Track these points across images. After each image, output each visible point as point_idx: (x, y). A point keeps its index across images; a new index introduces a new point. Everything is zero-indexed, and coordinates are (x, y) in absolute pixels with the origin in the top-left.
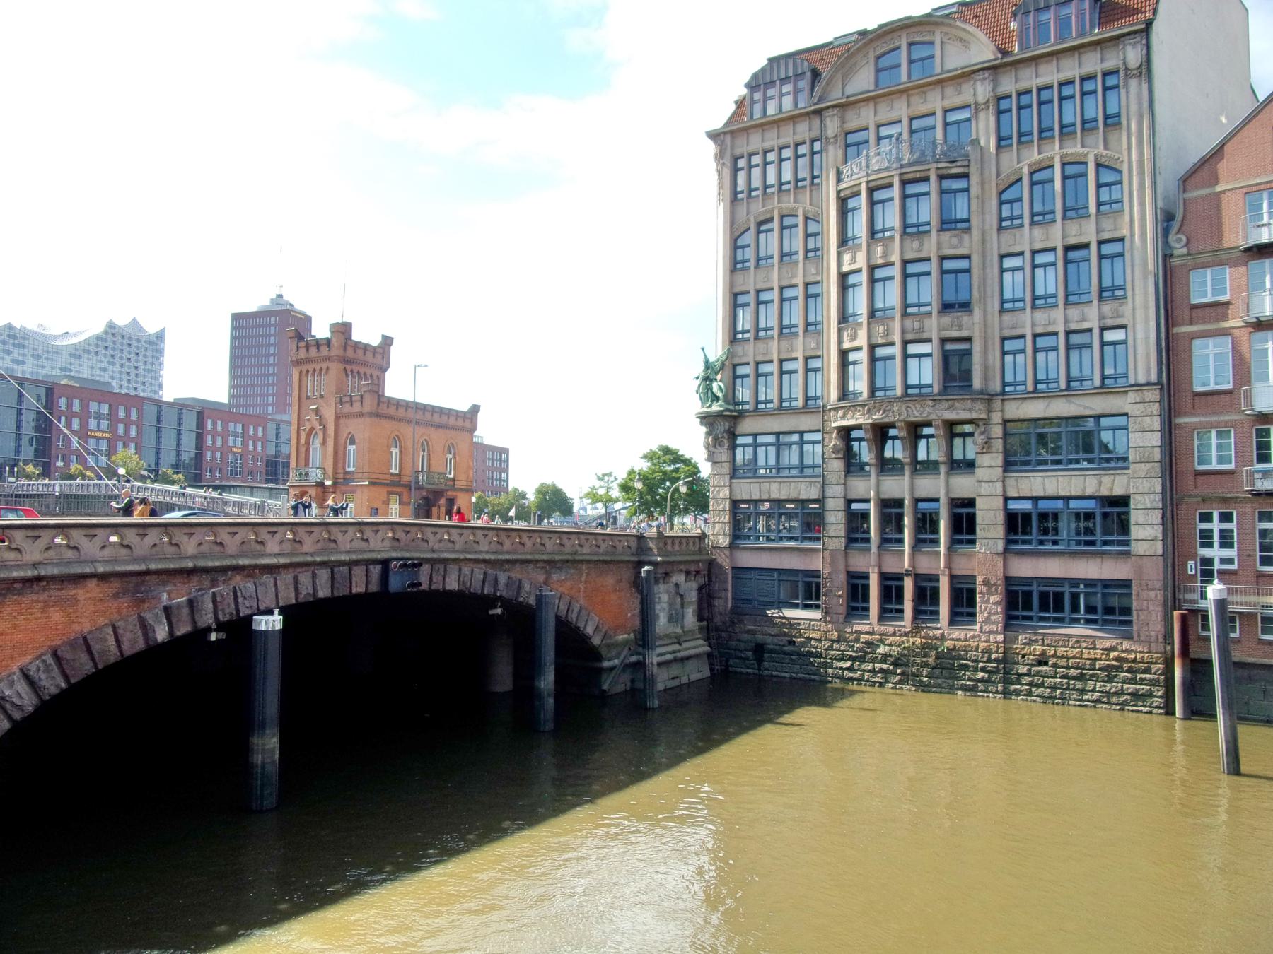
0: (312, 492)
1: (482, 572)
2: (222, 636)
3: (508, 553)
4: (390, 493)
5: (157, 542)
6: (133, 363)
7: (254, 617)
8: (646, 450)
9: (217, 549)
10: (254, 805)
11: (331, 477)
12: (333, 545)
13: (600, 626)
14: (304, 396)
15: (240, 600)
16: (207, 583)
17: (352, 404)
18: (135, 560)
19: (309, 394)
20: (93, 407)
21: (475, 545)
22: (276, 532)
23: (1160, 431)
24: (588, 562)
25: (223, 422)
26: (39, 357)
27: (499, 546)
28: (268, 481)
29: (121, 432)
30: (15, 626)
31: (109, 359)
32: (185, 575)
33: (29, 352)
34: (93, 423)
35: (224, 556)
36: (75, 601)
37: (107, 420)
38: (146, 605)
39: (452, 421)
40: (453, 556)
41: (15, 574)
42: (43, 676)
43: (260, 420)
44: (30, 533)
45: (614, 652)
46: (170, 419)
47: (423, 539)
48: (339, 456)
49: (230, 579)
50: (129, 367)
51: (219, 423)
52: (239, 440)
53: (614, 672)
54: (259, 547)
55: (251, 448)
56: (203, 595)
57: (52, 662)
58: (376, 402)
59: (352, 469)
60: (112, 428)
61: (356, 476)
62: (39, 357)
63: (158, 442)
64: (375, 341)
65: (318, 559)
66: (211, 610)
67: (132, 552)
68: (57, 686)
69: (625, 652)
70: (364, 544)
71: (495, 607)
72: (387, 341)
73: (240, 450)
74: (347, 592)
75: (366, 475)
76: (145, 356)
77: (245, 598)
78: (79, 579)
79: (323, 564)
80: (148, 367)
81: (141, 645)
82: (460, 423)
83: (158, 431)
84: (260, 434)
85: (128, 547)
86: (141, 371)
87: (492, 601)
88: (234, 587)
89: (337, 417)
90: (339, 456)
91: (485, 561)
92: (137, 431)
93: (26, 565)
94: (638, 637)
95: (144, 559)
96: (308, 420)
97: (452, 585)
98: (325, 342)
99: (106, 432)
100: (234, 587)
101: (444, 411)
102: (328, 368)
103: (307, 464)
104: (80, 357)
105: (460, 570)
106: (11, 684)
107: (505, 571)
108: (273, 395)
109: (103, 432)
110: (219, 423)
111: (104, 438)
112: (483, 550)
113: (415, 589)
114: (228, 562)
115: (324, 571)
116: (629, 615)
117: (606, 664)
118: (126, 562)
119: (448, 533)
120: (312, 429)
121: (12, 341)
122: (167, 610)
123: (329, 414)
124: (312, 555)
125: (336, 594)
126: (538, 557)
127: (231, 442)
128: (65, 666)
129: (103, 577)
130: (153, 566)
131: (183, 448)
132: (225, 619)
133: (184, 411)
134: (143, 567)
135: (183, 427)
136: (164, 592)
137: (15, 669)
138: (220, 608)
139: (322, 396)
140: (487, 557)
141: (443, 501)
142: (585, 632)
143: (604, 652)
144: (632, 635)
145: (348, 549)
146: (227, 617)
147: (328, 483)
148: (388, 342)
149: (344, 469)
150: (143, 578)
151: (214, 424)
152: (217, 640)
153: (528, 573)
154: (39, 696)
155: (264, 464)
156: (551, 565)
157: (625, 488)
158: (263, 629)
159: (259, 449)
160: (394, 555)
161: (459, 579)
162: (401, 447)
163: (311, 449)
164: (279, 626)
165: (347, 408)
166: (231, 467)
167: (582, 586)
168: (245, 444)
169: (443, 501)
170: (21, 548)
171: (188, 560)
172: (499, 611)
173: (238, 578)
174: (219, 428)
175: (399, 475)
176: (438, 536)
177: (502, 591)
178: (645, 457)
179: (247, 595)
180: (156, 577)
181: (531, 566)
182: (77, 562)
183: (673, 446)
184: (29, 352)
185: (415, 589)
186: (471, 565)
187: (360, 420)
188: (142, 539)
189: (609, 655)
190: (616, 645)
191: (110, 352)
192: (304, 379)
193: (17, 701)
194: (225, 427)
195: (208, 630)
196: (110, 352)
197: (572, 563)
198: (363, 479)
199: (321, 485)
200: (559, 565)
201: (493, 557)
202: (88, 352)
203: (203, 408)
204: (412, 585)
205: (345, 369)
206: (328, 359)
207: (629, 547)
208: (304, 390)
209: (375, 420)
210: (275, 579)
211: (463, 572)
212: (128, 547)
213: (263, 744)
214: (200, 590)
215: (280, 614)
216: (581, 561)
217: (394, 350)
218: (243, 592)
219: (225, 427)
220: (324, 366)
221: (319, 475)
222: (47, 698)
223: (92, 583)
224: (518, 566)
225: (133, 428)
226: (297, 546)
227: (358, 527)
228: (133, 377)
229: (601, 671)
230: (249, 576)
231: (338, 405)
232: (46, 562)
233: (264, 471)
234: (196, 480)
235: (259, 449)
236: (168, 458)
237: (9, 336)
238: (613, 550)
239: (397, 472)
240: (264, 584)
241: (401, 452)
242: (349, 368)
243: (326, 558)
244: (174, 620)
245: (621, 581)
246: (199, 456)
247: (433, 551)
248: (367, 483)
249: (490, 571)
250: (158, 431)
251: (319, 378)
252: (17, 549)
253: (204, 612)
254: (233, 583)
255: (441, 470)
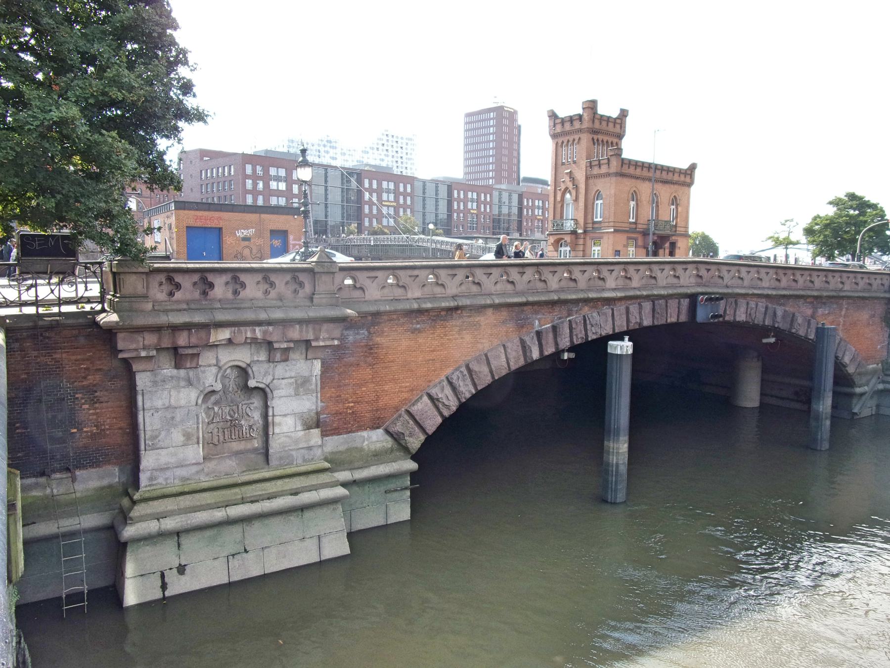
0: (568, 238)
1: (765, 306)
2: (572, 355)
3: (784, 289)
4: (629, 238)
5: (532, 279)
6: (400, 155)
7: (610, 342)
8: (832, 198)
9: (572, 284)
10: (609, 497)
11: (583, 226)
12: (653, 281)
13: (856, 357)
14: (559, 162)
15: (589, 327)
16: (565, 313)
17: (600, 167)
18: (518, 294)
19: (564, 161)
20: (385, 184)
21: (759, 282)
22: (613, 270)
23: (278, 168)
24: (849, 297)
25: (464, 192)
26: (344, 154)
27: (777, 283)
28: (494, 234)
29: (401, 201)
30: (442, 344)
31: (385, 152)
32: (550, 306)
33: (338, 151)
34: (385, 196)
35: (577, 291)
36: (477, 325)
37: (393, 193)
38: (524, 330)
39: (676, 178)
40: (743, 291)
41: (443, 305)
42: (461, 384)
43: (488, 189)
44: (451, 272)
45: (864, 380)
46: (430, 192)
47: (719, 277)
48: (588, 209)
49: (581, 309)
50: (397, 157)
51: (462, 192)
52: (475, 204)
53: (864, 398)
54: (601, 283)
55: (482, 209)
56: (562, 323)
57: (467, 373)
58: (620, 164)
59: (599, 219)
60: (396, 199)
61: (603, 225)
62: (344, 154)
63: (424, 208)
64: (615, 114)
65: (645, 293)
66: (568, 335)
67: (515, 286)
68: (470, 391)
69: (874, 381)
70: (675, 281)
71: (768, 337)
72: (624, 114)
73: (475, 212)
74: (663, 322)
75: (612, 224)
76: (406, 149)
77: (592, 326)
78: (481, 309)
79: (647, 297)
80: (409, 156)
81: (522, 362)
82: (682, 178)
83: (424, 200)
84: (488, 199)
85: (512, 283)
86: (404, 160)
87: (765, 331)
88: (584, 316)
89: (587, 178)
90: (588, 209)
91: (767, 297)
92: (411, 201)
93: (448, 297)
94: (885, 367)
95: (522, 293)
96: (563, 182)
97: (741, 317)
98: (577, 117)
99: (393, 202)
100: (584, 316)
101: (670, 169)
102: (580, 139)
103: (562, 217)
104: (368, 153)
105: (748, 303)
106: (442, 389)
107: (781, 305)
108: (492, 171)
109: (391, 202)
110: (462, 192)
111: (391, 206)
112: (765, 286)
113: (716, 320)
114: (581, 296)
115: (648, 303)
116: (879, 347)
117: (858, 390)
118: (510, 295)
119: (718, 269)
120: (567, 189)
121: (329, 144)
122: (539, 334)
123: (580, 176)
124: (639, 289)
125: (656, 323)
126: (809, 293)
127: (469, 206)
128: (474, 376)
129: (497, 307)
130: (531, 299)
131: (440, 211)
132: (578, 343)
133: (440, 185)
134: (524, 300)
135: (427, 195)
136: (536, 319)
137: (443, 378)
138: (575, 333)
139: (574, 162)
140: (770, 292)
141: (667, 245)
142: (842, 361)
143: (857, 380)
144: (880, 365)
145: (664, 285)
146: (580, 341)
147: (580, 231)
148: (625, 113)
149: (593, 219)
150: (522, 308)
151: (459, 194)
152: (569, 359)
153: (799, 307)
154: (458, 399)
155: (491, 221)
156: (818, 300)
157: (809, 232)
158: (619, 353)
159: (488, 210)
160: (700, 290)
161: (747, 313)
162: (637, 200)
163: (565, 205)
164: (630, 351)
165: (596, 171)
166: (470, 224)
167: (841, 320)
168: (478, 207)
169: (667, 245)
170: (577, 279)
171: (553, 294)
172: (772, 340)
173: (586, 308)
174: (462, 196)
175: (635, 223)
176: (732, 273)
177: (781, 324)
178: (830, 203)
179: (594, 323)
180: (530, 307)
181: (802, 301)
182: (480, 295)
183: (859, 193)
184: (338, 151)
185: (716, 320)
186: (755, 299)
187: (607, 179)
188: (685, 272)
189: (860, 382)
190: (866, 374)
191: (385, 147)
192: (560, 148)
193: (447, 403)
194: (466, 195)
195: (563, 351)
196: (385, 147)
197: (836, 299)
198: (609, 227)
199: (574, 233)
200: (824, 300)
201: (774, 293)
202: (373, 149)
203: (451, 183)
204: (714, 317)
205: (593, 139)
206: (580, 131)
207: (882, 285)
208: (560, 158)
209: (620, 179)
210: (613, 310)
211: (750, 306)
212: (512, 283)
213: (618, 448)
214: (560, 318)
215: (630, 340)
216: (843, 297)
217: (628, 120)
218: (591, 320)
219: (466, 195)
220: (576, 137)
221: (572, 225)
222: (464, 400)
223: (490, 311)
224: (791, 302)
225: (409, 199)
226: (628, 281)
227: (672, 265)
228: (399, 164)
229: (851, 395)
230: (595, 307)
231: (588, 168)
232: (460, 294)
233: (491, 226)
234: (448, 233)
235: (488, 210)
236: (431, 217)
237: (327, 141)
238: (869, 287)
239: (634, 221)
240: (605, 314)
241: (637, 204)
242: (595, 137)
243: (649, 293)
244: (544, 342)
245: (873, 316)
246: (450, 216)
247: (727, 287)
248: (612, 230)
249: (770, 305)
250: (424, 200)
251: (566, 148)
252: (443, 285)
253: (563, 336)
254: (583, 313)
255: (667, 219)
